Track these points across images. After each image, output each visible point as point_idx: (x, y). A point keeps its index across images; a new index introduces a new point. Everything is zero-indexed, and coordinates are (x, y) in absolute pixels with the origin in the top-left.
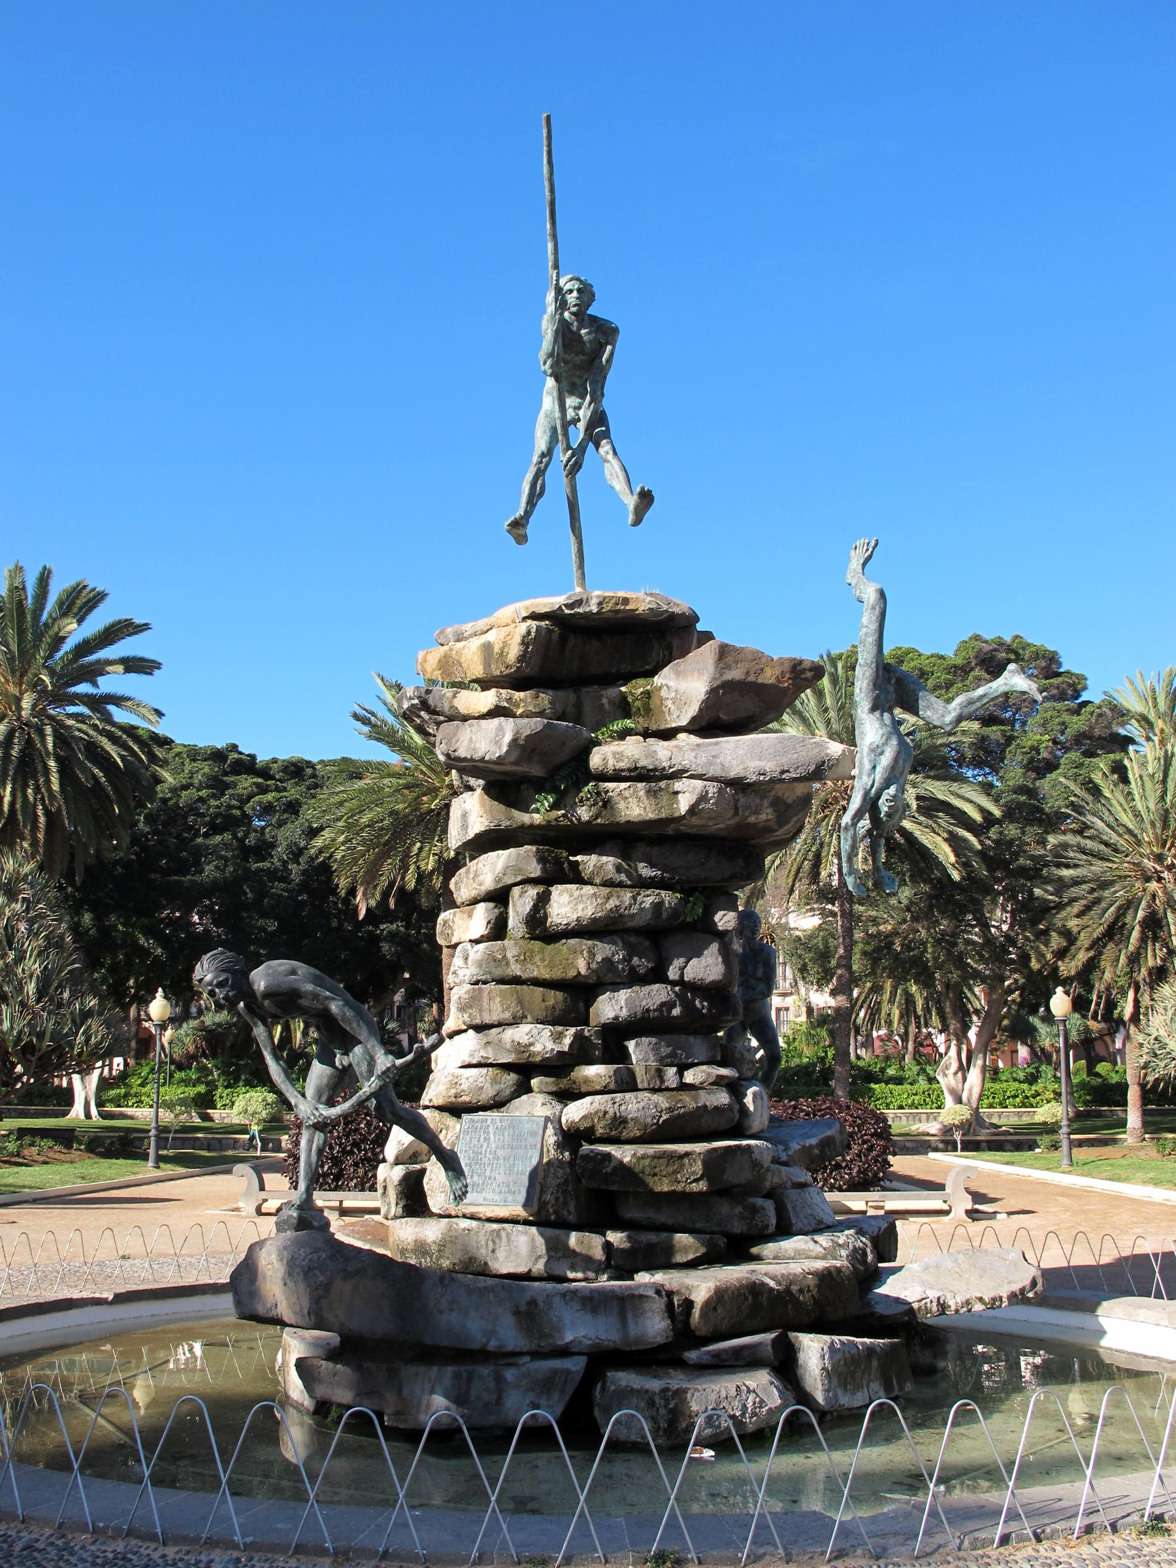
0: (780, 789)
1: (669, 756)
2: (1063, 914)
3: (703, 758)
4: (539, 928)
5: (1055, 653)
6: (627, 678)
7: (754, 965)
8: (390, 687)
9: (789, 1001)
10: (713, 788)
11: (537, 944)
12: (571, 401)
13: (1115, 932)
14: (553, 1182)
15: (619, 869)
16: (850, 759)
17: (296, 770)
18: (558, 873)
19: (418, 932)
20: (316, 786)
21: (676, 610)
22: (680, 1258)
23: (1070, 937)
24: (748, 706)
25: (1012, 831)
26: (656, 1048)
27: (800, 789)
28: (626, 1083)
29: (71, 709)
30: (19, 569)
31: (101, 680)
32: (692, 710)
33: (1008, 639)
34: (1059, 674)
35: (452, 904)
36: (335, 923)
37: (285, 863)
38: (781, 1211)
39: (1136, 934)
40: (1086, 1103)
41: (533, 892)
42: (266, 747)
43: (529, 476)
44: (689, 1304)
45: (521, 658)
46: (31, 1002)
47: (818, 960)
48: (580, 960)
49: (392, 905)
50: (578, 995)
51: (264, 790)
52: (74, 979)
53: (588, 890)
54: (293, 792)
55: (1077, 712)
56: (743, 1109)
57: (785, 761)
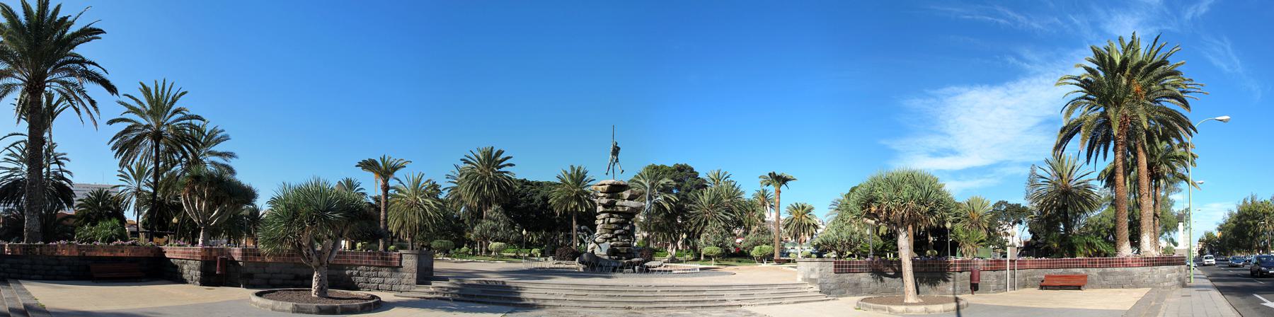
1: (625, 203)
7: (633, 228)
13: (699, 223)
17: (538, 184)
47: (645, 227)
50: (613, 230)
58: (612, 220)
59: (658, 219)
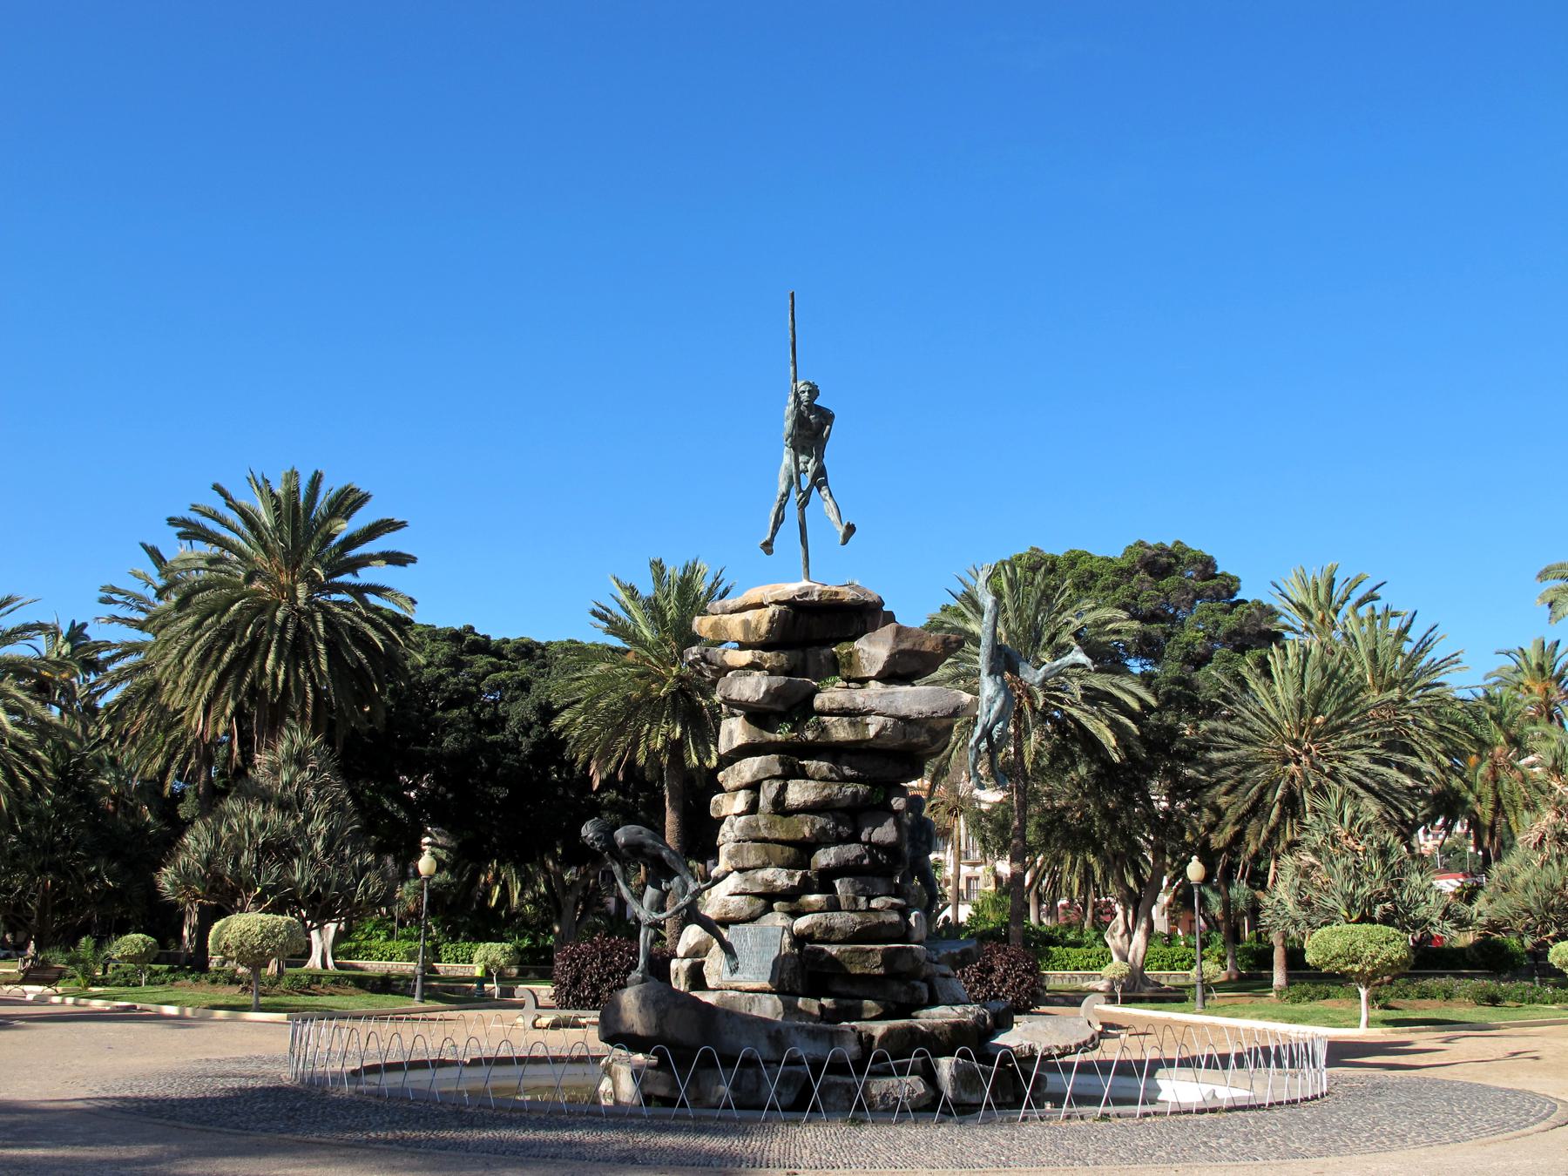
0: (932, 723)
1: (865, 698)
2: (1213, 792)
3: (884, 703)
4: (780, 807)
5: (1211, 558)
6: (836, 642)
7: (922, 834)
8: (625, 588)
9: (979, 870)
10: (890, 722)
11: (778, 818)
12: (802, 458)
13: (1257, 808)
14: (788, 967)
15: (831, 770)
16: (975, 703)
17: (527, 650)
18: (795, 772)
19: (636, 801)
20: (544, 666)
21: (869, 599)
22: (866, 1015)
23: (1218, 812)
24: (915, 665)
25: (1169, 718)
26: (853, 885)
27: (945, 722)
28: (834, 906)
29: (335, 597)
30: (294, 474)
31: (359, 572)
32: (879, 667)
33: (1169, 545)
34: (1214, 576)
35: (721, 790)
36: (560, 791)
37: (516, 736)
38: (932, 990)
39: (1275, 811)
40: (1248, 967)
41: (776, 784)
42: (498, 627)
43: (774, 509)
44: (871, 1038)
45: (769, 631)
46: (320, 857)
47: (998, 833)
48: (805, 828)
49: (621, 777)
50: (802, 851)
51: (498, 669)
52: (356, 837)
53: (812, 783)
54: (524, 671)
55: (1228, 611)
56: (909, 925)
57: (935, 705)
58: (797, 793)
59: (1064, 792)
